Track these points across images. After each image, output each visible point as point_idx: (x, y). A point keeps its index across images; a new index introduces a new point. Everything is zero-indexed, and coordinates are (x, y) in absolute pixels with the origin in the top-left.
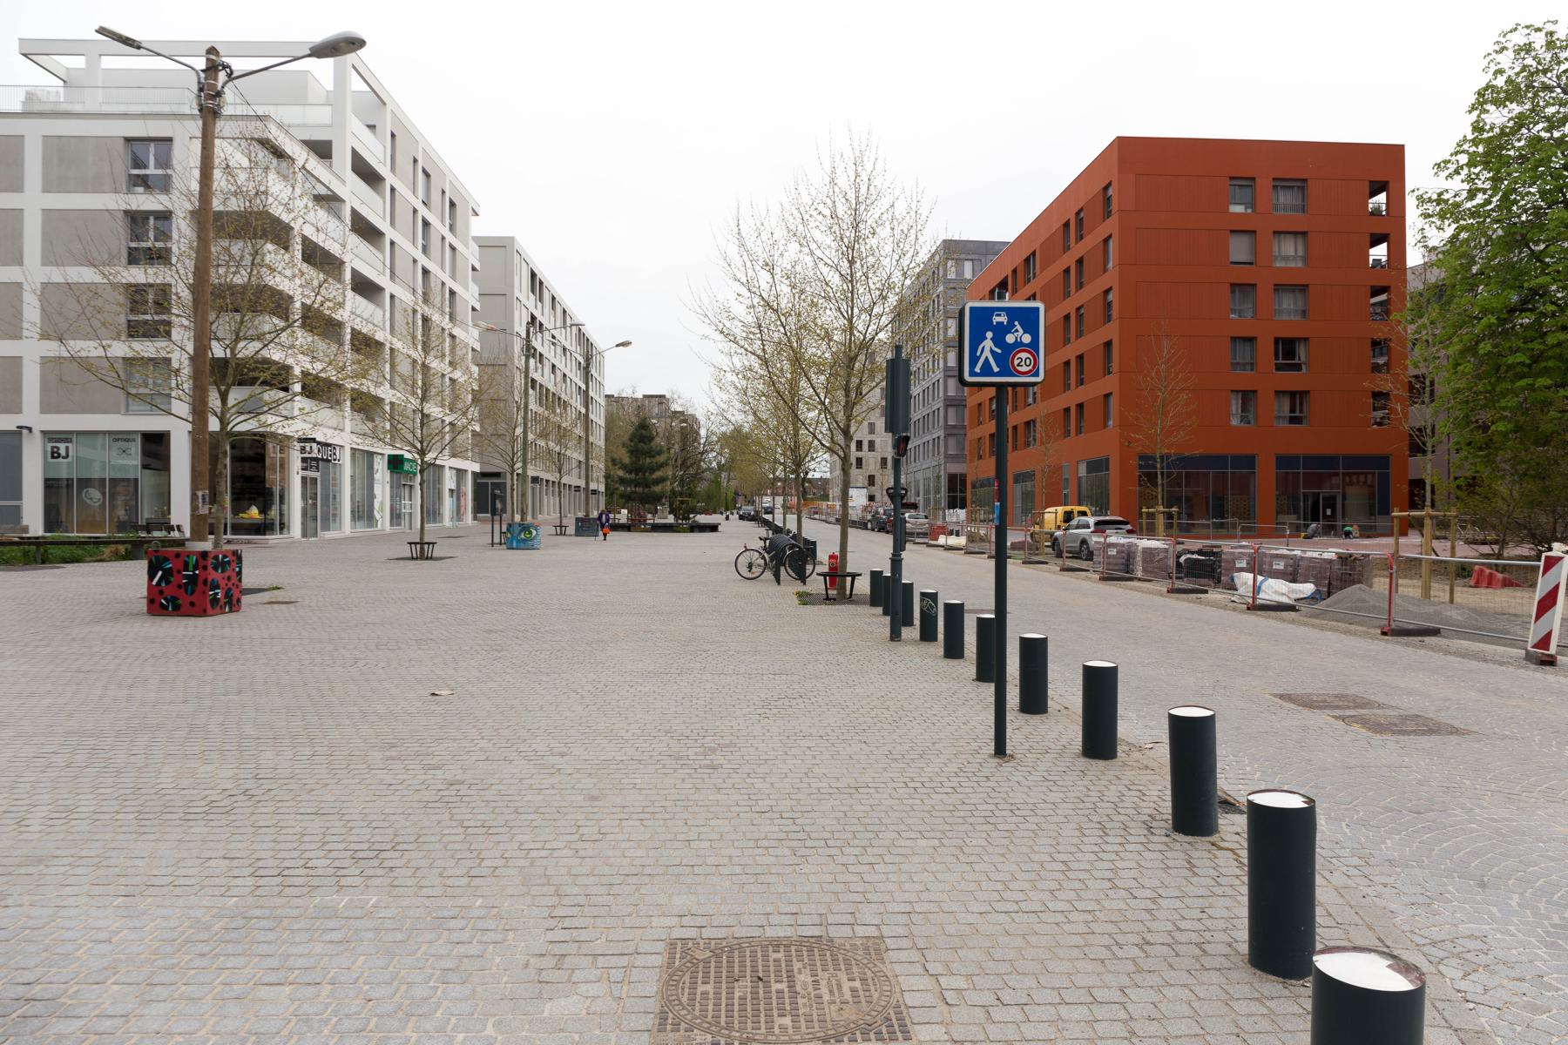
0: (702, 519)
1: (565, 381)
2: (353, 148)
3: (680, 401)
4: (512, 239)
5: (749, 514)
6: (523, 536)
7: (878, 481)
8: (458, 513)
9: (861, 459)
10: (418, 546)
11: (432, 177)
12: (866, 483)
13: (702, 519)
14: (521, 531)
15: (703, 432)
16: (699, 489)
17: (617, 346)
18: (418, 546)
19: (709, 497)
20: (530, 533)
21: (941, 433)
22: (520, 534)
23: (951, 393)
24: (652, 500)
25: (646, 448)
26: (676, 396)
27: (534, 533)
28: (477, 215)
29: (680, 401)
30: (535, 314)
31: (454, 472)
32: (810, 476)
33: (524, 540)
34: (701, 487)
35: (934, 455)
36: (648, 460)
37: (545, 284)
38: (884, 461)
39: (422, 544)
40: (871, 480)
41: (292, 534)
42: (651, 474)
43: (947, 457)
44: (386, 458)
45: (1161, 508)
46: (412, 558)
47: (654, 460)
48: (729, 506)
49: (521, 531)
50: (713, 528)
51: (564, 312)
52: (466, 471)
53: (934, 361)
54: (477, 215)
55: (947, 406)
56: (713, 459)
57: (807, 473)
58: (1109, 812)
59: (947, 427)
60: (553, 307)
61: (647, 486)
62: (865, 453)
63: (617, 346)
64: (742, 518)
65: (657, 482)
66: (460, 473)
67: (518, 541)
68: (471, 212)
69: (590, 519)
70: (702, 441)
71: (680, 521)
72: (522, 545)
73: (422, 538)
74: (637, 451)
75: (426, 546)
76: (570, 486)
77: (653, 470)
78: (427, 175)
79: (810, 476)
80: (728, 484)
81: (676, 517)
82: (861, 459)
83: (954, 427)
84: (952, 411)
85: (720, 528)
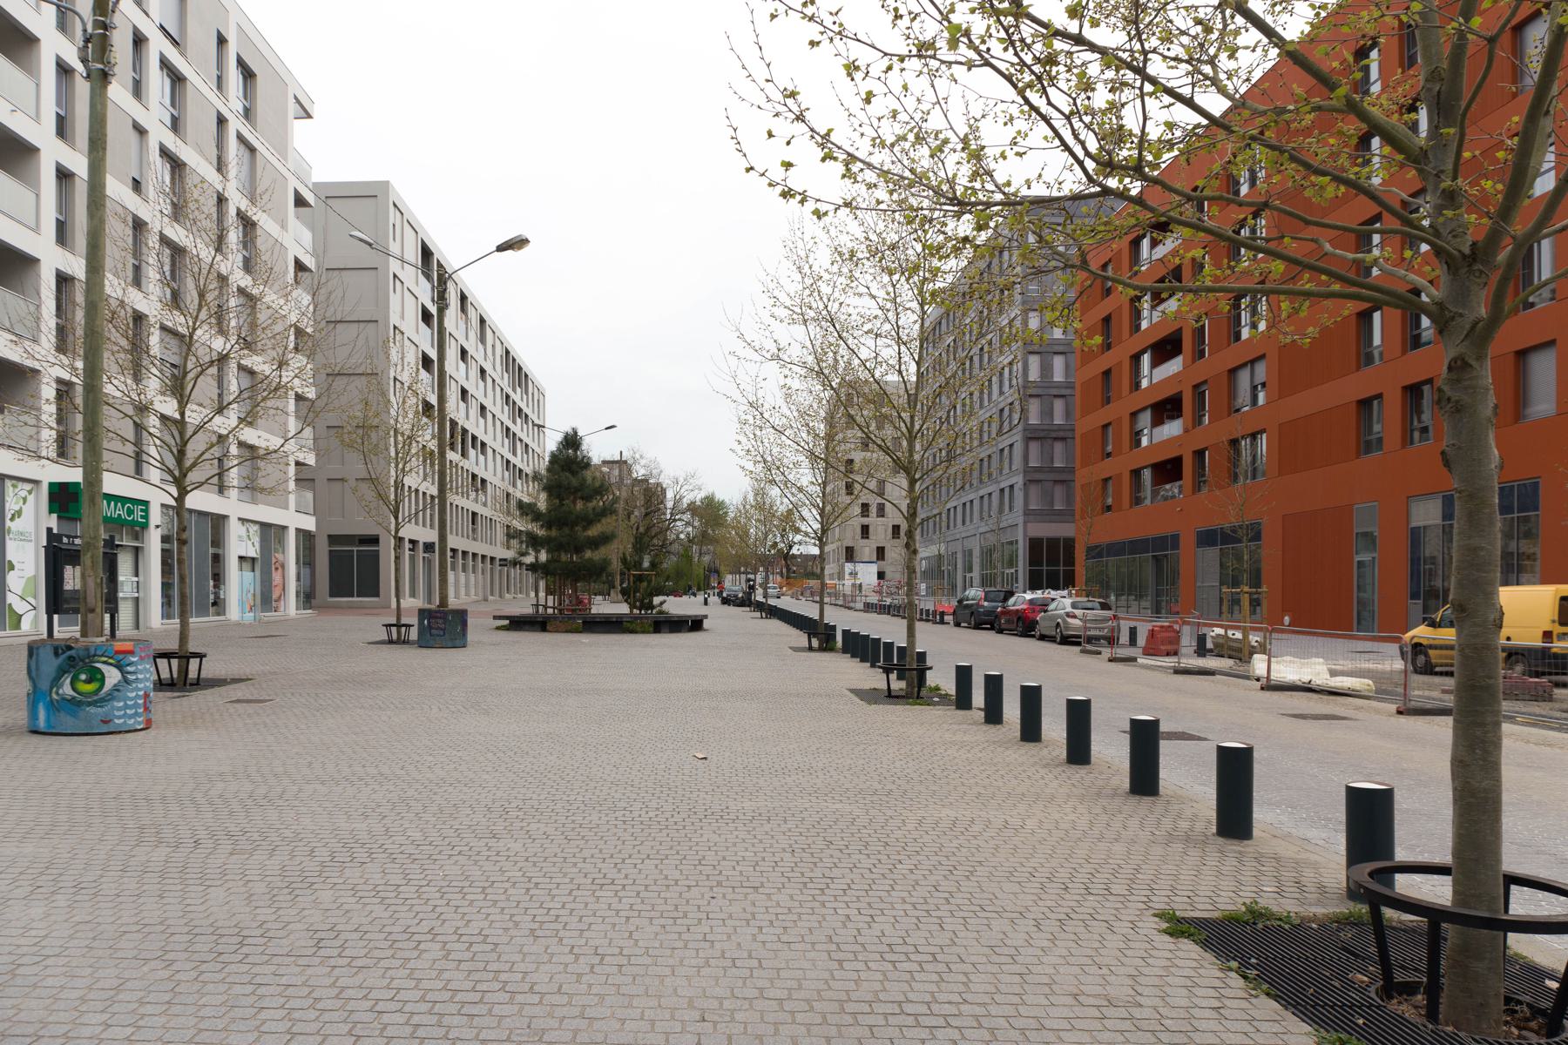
0: (677, 606)
1: (527, 452)
2: (161, 53)
3: (643, 462)
4: (385, 185)
5: (736, 596)
6: (67, 690)
7: (888, 554)
8: (267, 598)
9: (867, 526)
10: (175, 662)
11: (259, 79)
12: (874, 558)
13: (677, 606)
14: (61, 672)
15: (670, 495)
16: (665, 565)
17: (501, 248)
18: (175, 662)
19: (679, 574)
20: (96, 677)
21: (1018, 480)
22: (56, 681)
23: (1034, 420)
24: (596, 576)
25: (574, 482)
26: (637, 456)
27: (112, 676)
28: (309, 116)
29: (643, 462)
30: (467, 347)
31: (255, 528)
32: (794, 551)
33: (75, 704)
34: (669, 563)
35: (964, 522)
36: (579, 505)
37: (470, 299)
38: (896, 529)
39: (399, 626)
40: (881, 552)
41: (228, 616)
42: (585, 529)
43: (1027, 513)
44: (45, 490)
45: (1246, 589)
46: (391, 642)
47: (591, 505)
48: (703, 582)
49: (61, 672)
50: (696, 624)
51: (482, 321)
52: (284, 528)
53: (982, 392)
54: (309, 116)
55: (1028, 439)
56: (683, 529)
57: (791, 547)
58: (1117, 924)
59: (1027, 470)
60: (463, 309)
61: (578, 550)
62: (872, 519)
63: (501, 248)
64: (725, 601)
65: (595, 543)
66: (271, 533)
67: (54, 707)
68: (292, 107)
69: (445, 614)
70: (670, 504)
71: (635, 611)
72: (67, 722)
73: (399, 618)
74: (559, 486)
75: (403, 629)
76: (492, 559)
77: (589, 521)
78: (248, 74)
79: (794, 551)
80: (702, 559)
81: (632, 607)
82: (867, 526)
83: (1037, 470)
84: (1034, 447)
85: (706, 623)
